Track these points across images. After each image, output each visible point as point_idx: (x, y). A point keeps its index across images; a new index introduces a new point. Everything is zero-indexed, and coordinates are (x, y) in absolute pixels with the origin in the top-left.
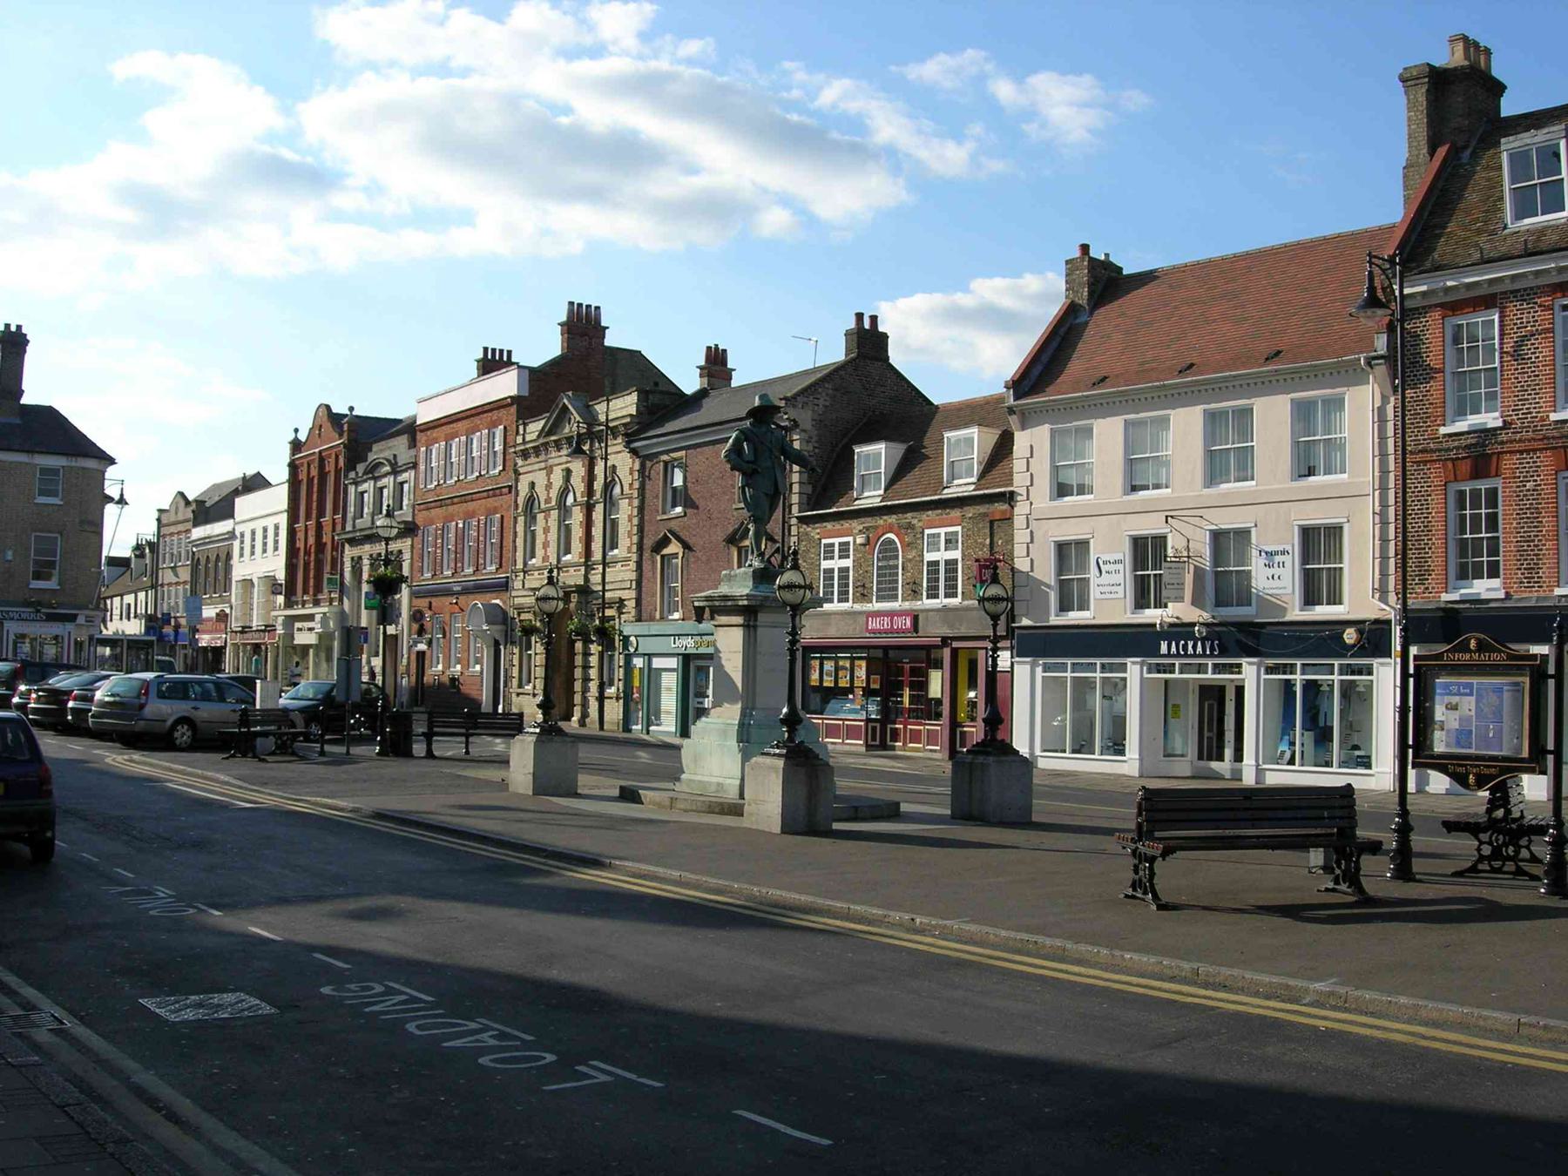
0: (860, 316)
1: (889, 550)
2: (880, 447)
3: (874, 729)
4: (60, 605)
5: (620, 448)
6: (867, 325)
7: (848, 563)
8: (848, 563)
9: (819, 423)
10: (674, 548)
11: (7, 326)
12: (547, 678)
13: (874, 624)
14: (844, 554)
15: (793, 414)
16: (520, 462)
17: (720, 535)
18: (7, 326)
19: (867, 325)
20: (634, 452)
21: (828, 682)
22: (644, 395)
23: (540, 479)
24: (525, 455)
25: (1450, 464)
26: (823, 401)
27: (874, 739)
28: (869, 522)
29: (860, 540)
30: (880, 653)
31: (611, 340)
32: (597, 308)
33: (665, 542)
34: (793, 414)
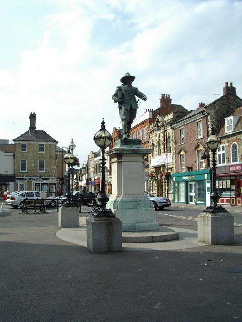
0: (227, 83)
1: (235, 147)
2: (231, 117)
3: (233, 200)
4: (45, 176)
5: (170, 128)
6: (229, 85)
7: (224, 152)
8: (224, 152)
9: (216, 114)
10: (183, 152)
11: (32, 113)
12: (158, 189)
13: (231, 169)
14: (223, 149)
15: (208, 111)
16: (150, 135)
17: (193, 147)
18: (32, 113)
19: (229, 85)
20: (172, 128)
21: (221, 187)
22: (175, 113)
23: (154, 138)
24: (151, 133)
25: (219, 184)
26: (217, 107)
27: (233, 203)
28: (229, 139)
29: (227, 145)
30: (233, 178)
31: (173, 103)
32: (169, 95)
33: (181, 151)
34: (208, 111)
